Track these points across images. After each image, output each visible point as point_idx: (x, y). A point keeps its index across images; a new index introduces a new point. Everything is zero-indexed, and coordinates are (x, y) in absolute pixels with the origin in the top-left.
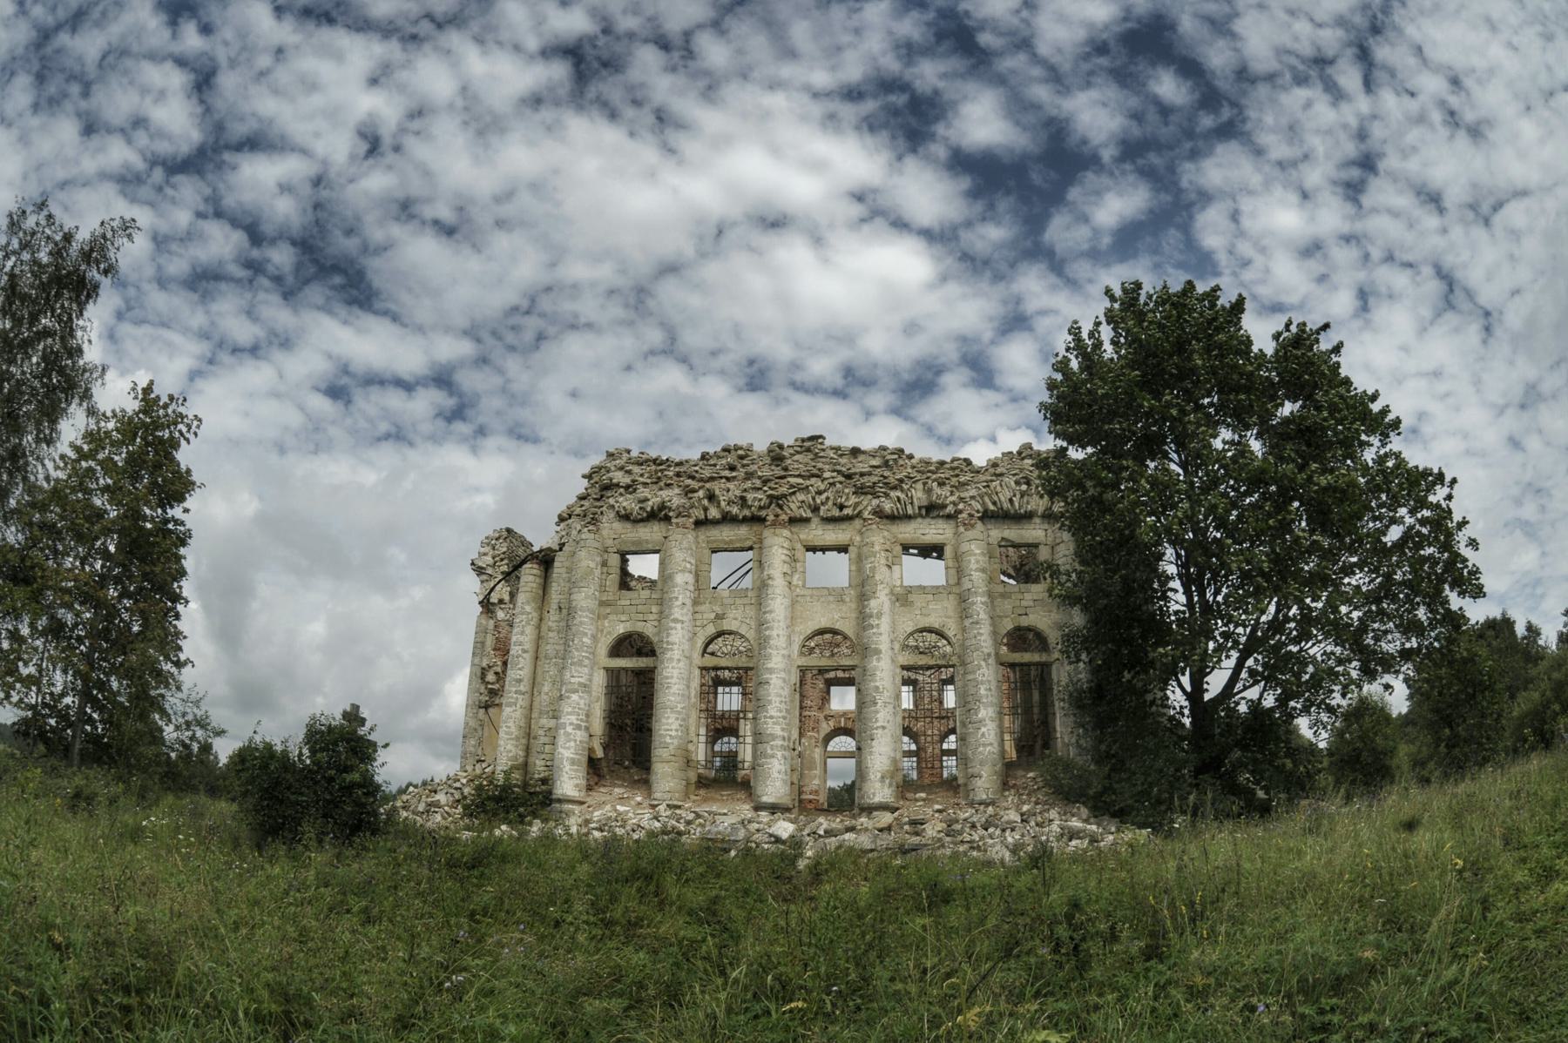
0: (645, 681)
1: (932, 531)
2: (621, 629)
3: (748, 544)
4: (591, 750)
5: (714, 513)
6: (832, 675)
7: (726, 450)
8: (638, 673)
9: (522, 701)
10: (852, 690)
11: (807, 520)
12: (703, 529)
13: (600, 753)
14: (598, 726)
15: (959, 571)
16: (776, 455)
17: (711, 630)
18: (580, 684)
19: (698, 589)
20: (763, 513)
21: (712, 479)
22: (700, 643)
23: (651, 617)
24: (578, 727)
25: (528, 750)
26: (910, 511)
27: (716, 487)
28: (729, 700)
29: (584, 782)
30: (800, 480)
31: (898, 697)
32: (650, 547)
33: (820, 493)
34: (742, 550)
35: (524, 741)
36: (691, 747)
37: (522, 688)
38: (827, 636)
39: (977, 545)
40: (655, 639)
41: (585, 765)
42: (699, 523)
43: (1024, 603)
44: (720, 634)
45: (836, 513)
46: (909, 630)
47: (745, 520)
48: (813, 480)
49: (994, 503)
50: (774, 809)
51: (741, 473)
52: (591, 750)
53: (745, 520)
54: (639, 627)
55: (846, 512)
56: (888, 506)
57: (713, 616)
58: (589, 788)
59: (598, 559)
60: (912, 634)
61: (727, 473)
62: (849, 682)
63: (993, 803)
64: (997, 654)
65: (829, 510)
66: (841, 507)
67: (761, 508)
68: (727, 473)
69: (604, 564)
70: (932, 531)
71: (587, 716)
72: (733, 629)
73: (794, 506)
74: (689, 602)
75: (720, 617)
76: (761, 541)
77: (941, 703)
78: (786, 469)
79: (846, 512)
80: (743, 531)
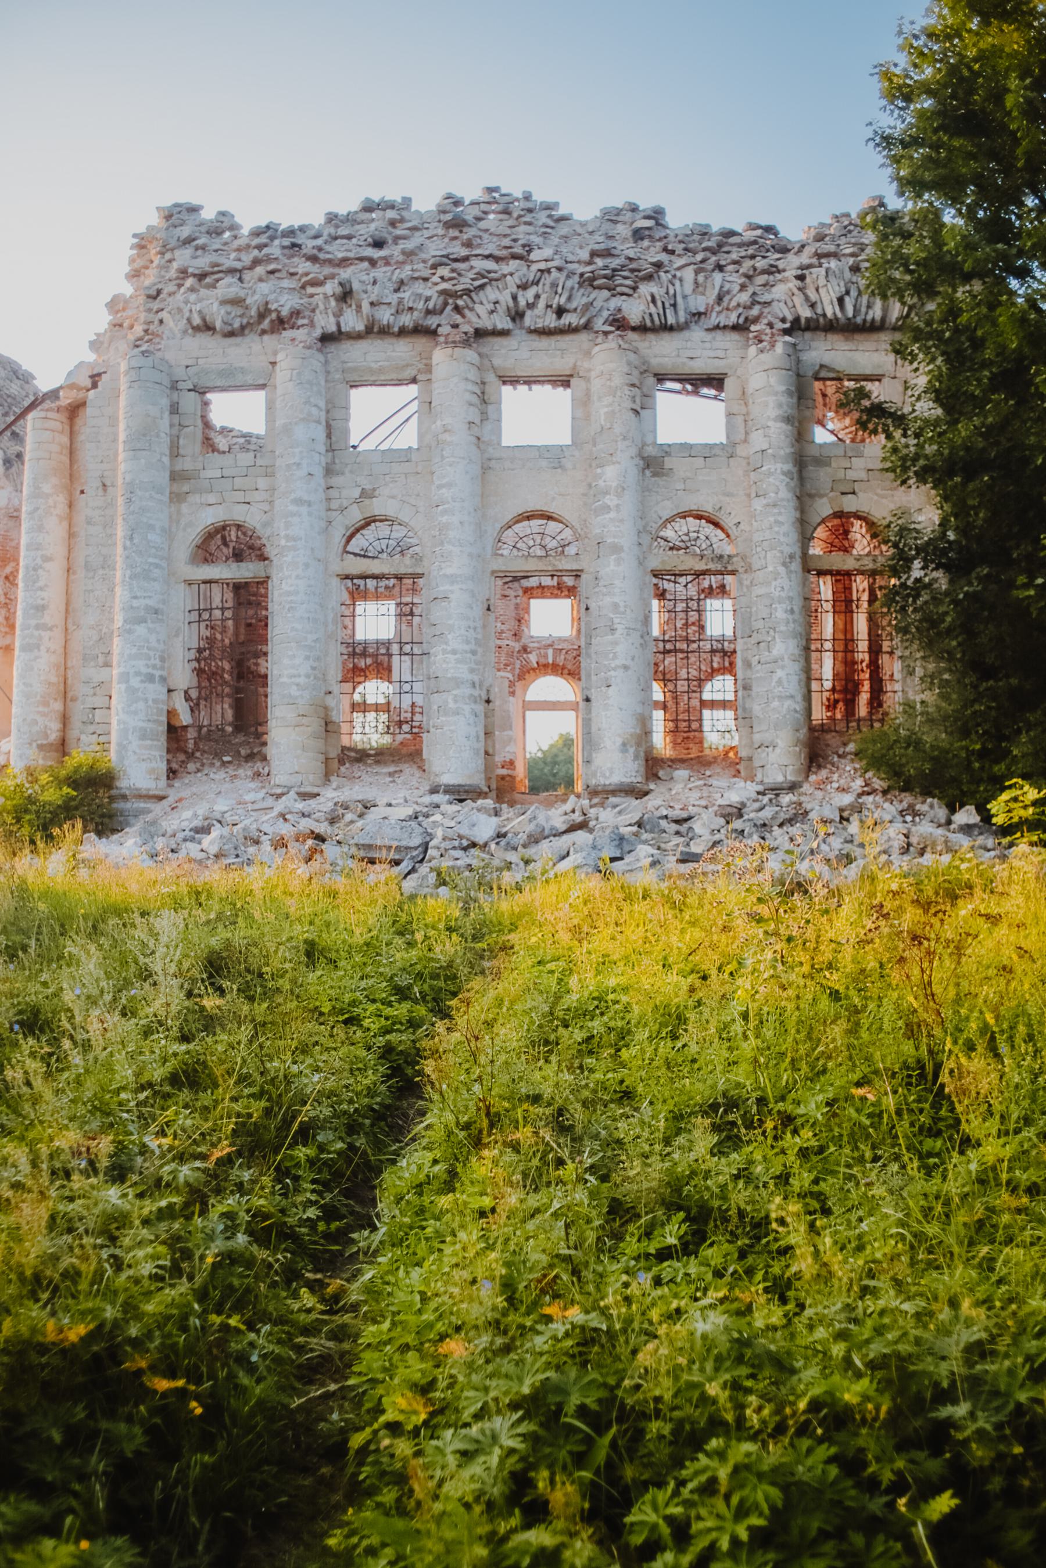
0: (249, 597)
1: (698, 350)
2: (210, 517)
3: (409, 373)
4: (171, 713)
5: (352, 321)
6: (533, 582)
7: (369, 207)
8: (239, 588)
9: (52, 641)
10: (564, 605)
11: (504, 333)
12: (332, 348)
13: (185, 718)
14: (184, 677)
15: (739, 420)
16: (454, 219)
17: (356, 515)
18: (148, 608)
19: (331, 449)
20: (432, 321)
21: (344, 262)
22: (338, 535)
23: (257, 496)
24: (150, 678)
25: (65, 720)
26: (671, 320)
27: (355, 275)
28: (375, 621)
29: (163, 766)
30: (490, 265)
31: (647, 620)
32: (249, 379)
33: (523, 287)
34: (399, 383)
35: (58, 706)
36: (330, 701)
37: (47, 619)
38: (535, 523)
39: (761, 373)
40: (260, 532)
41: (163, 738)
42: (326, 339)
43: (851, 475)
44: (368, 522)
45: (550, 321)
46: (666, 514)
47: (403, 332)
48: (514, 264)
49: (813, 306)
50: (461, 794)
51: (392, 251)
52: (171, 713)
53: (403, 332)
54: (239, 514)
55: (568, 319)
56: (635, 310)
57: (357, 493)
58: (172, 773)
59: (165, 402)
60: (670, 520)
61: (371, 252)
62: (562, 590)
63: (793, 787)
64: (805, 556)
65: (540, 317)
66: (560, 312)
67: (428, 312)
68: (371, 252)
69: (174, 409)
70: (698, 350)
71: (163, 659)
72: (390, 512)
73: (481, 316)
74: (319, 472)
75: (366, 494)
76: (429, 369)
77: (702, 628)
78: (468, 244)
79: (568, 319)
80: (403, 350)
